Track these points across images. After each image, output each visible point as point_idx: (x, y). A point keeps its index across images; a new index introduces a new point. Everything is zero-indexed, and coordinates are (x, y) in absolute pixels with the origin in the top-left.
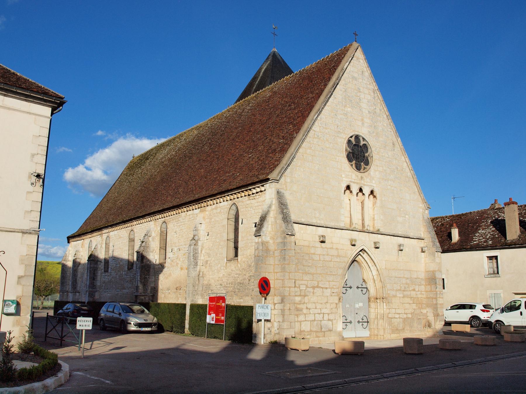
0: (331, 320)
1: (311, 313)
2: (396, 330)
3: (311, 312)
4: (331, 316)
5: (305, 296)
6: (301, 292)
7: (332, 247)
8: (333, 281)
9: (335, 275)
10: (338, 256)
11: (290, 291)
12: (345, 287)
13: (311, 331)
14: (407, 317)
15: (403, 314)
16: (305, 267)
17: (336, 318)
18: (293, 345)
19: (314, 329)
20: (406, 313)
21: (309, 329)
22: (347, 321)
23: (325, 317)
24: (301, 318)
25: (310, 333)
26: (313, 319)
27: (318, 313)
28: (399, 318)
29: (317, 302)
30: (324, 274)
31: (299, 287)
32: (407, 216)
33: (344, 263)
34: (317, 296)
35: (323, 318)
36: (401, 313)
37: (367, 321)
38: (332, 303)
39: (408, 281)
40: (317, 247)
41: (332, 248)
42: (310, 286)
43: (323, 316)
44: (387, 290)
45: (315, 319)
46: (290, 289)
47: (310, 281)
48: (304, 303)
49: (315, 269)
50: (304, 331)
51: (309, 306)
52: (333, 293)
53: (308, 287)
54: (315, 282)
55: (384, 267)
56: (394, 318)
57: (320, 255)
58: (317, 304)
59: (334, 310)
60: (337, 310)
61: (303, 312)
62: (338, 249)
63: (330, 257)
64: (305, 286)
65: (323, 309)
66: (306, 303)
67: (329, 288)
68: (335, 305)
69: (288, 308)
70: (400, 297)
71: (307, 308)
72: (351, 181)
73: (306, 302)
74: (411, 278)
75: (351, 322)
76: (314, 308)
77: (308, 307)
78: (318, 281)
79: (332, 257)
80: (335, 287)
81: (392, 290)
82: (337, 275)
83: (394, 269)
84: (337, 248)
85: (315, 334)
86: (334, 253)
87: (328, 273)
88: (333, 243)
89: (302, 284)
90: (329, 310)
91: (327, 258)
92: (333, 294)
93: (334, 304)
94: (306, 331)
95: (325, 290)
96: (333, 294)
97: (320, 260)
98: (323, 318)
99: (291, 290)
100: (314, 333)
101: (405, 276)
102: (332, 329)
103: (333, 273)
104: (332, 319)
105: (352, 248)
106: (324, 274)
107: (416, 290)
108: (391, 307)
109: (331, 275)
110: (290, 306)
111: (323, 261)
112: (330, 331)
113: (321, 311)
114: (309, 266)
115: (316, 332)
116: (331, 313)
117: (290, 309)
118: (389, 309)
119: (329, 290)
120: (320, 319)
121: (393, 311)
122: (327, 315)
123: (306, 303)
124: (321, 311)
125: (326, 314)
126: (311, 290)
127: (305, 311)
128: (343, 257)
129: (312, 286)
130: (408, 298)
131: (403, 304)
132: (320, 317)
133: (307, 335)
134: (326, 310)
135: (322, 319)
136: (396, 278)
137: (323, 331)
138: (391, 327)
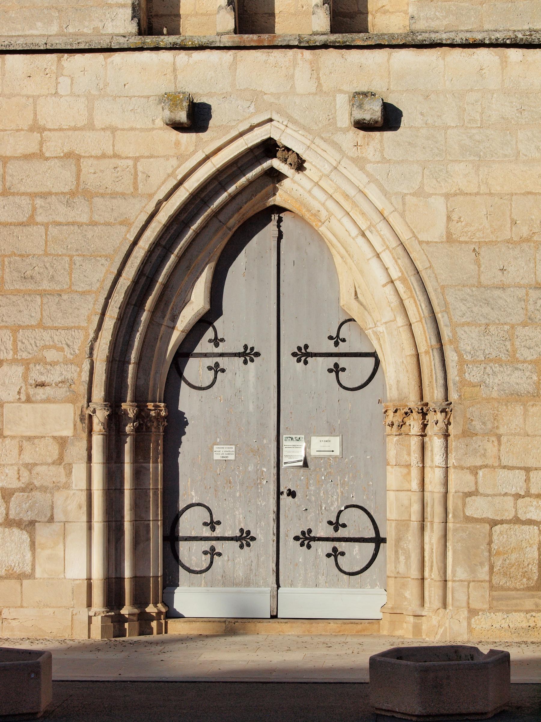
7: (33, 148)
8: (41, 325)
18: (515, 654)
22: (216, 534)
37: (372, 534)
38: (29, 439)
44: (462, 362)
56: (516, 521)
62: (78, 158)
63: (25, 201)
67: (14, 361)
68: (54, 450)
79: (39, 202)
80: (51, 355)
81: (498, 361)
83: (528, 240)
84: (69, 155)
88: (42, 129)
92: (41, 393)
96: (40, 390)
103: (45, 285)
105: (177, 144)
109: (29, 293)
118: (474, 471)
128: (114, 195)
138: (483, 573)
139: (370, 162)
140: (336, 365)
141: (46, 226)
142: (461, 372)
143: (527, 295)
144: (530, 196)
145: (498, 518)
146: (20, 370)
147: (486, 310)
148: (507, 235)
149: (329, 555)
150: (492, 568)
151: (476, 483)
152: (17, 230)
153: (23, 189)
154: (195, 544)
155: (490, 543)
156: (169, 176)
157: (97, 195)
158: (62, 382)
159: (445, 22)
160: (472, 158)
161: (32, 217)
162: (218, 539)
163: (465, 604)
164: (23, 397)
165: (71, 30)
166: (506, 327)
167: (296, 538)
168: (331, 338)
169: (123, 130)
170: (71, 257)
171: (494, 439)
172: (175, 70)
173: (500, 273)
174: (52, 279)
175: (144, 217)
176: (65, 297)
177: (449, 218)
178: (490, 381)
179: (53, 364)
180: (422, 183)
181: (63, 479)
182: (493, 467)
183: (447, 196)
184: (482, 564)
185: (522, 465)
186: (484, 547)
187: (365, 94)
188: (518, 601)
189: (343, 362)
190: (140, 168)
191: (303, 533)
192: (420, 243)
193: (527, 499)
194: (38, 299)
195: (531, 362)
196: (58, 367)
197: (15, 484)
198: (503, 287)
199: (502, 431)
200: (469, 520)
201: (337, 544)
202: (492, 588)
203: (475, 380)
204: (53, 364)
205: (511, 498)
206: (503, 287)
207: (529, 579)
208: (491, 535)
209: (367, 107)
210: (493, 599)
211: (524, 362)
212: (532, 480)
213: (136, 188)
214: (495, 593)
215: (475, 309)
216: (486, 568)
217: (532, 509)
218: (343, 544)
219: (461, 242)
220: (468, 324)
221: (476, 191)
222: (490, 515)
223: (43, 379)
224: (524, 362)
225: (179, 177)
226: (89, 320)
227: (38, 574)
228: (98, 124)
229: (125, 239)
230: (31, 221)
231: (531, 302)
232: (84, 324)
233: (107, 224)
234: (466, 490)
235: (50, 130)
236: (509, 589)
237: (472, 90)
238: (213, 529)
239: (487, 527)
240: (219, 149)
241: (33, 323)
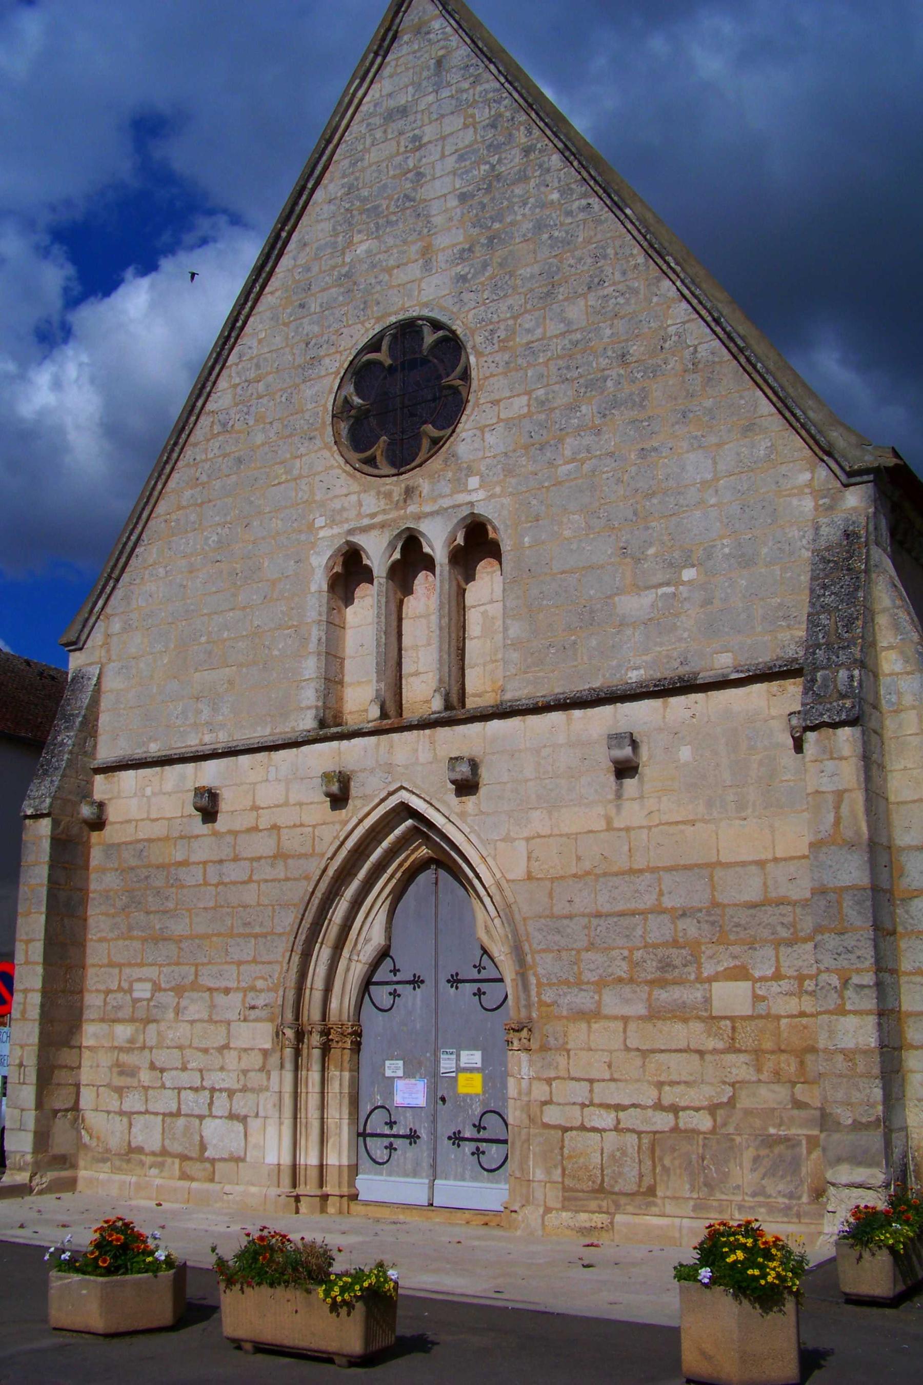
0: (243, 1119)
1: (168, 1084)
2: (594, 1191)
3: (168, 1078)
4: (242, 1104)
5: (148, 1021)
6: (134, 1007)
8: (255, 961)
9: (265, 935)
10: (280, 856)
11: (25, 1003)
12: (387, 983)
13: (164, 1152)
14: (675, 1129)
15: (650, 1112)
16: (152, 916)
17: (261, 1113)
19: (176, 1148)
20: (666, 1102)
21: (156, 1146)
23: (217, 1103)
24: (133, 1102)
25: (160, 1159)
26: (174, 1108)
27: (190, 1088)
28: (616, 1129)
29: (190, 1046)
30: (219, 935)
31: (130, 991)
32: (688, 574)
33: (304, 883)
34: (192, 1022)
35: (210, 1109)
36: (634, 1106)
38: (246, 1050)
39: (690, 928)
40: (197, 836)
41: (255, 829)
42: (168, 986)
43: (212, 1097)
44: (539, 984)
45: (179, 1109)
46: (26, 998)
47: (168, 965)
48: (143, 1048)
49: (187, 920)
50: (140, 1150)
51: (162, 1057)
52: (253, 1008)
53: (160, 989)
54: (187, 967)
55: (519, 872)
56: (583, 1128)
57: (205, 863)
58: (188, 1052)
59: (256, 1078)
60: (269, 1079)
61: (139, 1081)
63: (247, 863)
64: (149, 986)
65: (209, 1070)
66: (151, 1048)
67: (237, 989)
69: (17, 1061)
70: (625, 1019)
71: (153, 1067)
72: (351, 532)
73: (149, 1044)
74: (715, 904)
75: (413, 1137)
76: (177, 1069)
77: (158, 1064)
78: (197, 965)
79: (255, 864)
80: (260, 984)
81: (567, 983)
82: (272, 933)
85: (177, 1166)
86: (263, 845)
87: (235, 931)
89: (140, 980)
90: (234, 1075)
91: (234, 872)
92: (253, 1014)
93: (256, 1051)
94: (147, 1150)
95: (220, 999)
97: (206, 884)
98: (210, 1109)
99: (28, 1000)
100: (173, 1163)
101: (667, 902)
102: (242, 1154)
103: (257, 930)
104: (243, 1112)
106: (219, 935)
107: (757, 974)
108: (563, 1073)
109: (249, 935)
110: (22, 1056)
111: (217, 885)
112: (238, 1160)
113: (203, 1079)
114: (165, 912)
115: (184, 1158)
116: (244, 1089)
117: (21, 1065)
118: (549, 1081)
119: (236, 998)
120: (197, 1111)
121: (580, 1092)
122: (225, 1094)
123: (151, 1048)
124: (203, 1079)
125: (220, 1090)
126: (168, 998)
127: (145, 1077)
128: (300, 856)
129: (173, 984)
130: (685, 1020)
131: (645, 1053)
132: (197, 1102)
133: (150, 1168)
134: (223, 1075)
135: (207, 1113)
136: (601, 921)
137: (208, 1160)
138: (557, 1175)
139: (470, 815)
140: (479, 989)
141: (258, 882)
142: (539, 994)
143: (590, 922)
144: (591, 835)
145: (569, 1125)
146: (241, 995)
147: (557, 938)
148: (574, 870)
149: (473, 1154)
150: (564, 1170)
151: (551, 1092)
152: (241, 887)
153: (245, 856)
154: (379, 1140)
155: (562, 1148)
156: (335, 838)
157: (292, 857)
158: (266, 1005)
159: (526, 691)
160: (545, 805)
161: (251, 877)
162: (394, 1136)
163: (542, 1203)
164: (242, 1018)
165: (277, 731)
166: (574, 952)
167: (450, 1138)
168: (475, 966)
169: (307, 804)
170: (273, 906)
171: (565, 1053)
172: (340, 753)
173: (568, 904)
174: (261, 925)
175: (319, 872)
176: (269, 938)
177: (529, 858)
178: (561, 1001)
179: (261, 991)
180: (509, 830)
181: (265, 1083)
182: (564, 1079)
183: (528, 839)
184: (555, 1167)
185: (587, 1077)
186: (557, 1151)
187: (456, 759)
188: (585, 1202)
189: (484, 987)
190: (317, 833)
191: (454, 1133)
192: (508, 881)
193: (591, 1108)
194: (253, 941)
195: (593, 983)
196: (263, 994)
197: (236, 1086)
198: (570, 917)
199: (569, 1047)
200: (546, 1126)
201: (479, 1144)
202: (565, 1189)
203: (549, 1001)
204: (261, 991)
205: (578, 1107)
206: (570, 917)
207: (594, 1182)
208: (563, 1140)
209: (458, 769)
210: (565, 1199)
211: (588, 983)
212: (596, 1090)
213: (314, 850)
214: (566, 1194)
215: (550, 937)
216: (559, 1171)
217: (595, 1117)
218: (484, 1144)
219: (538, 879)
220: (544, 951)
221: (549, 832)
222: (563, 1123)
223: (253, 1003)
224: (588, 983)
225: (341, 839)
226: (283, 956)
227: (248, 1159)
228: (292, 801)
229: (307, 890)
230: (250, 880)
231: (593, 929)
232: (280, 959)
233: (295, 879)
234: (543, 1099)
235: (263, 808)
236: (577, 1191)
237: (545, 746)
238: (391, 1128)
239: (560, 1133)
240: (368, 814)
241: (249, 959)
